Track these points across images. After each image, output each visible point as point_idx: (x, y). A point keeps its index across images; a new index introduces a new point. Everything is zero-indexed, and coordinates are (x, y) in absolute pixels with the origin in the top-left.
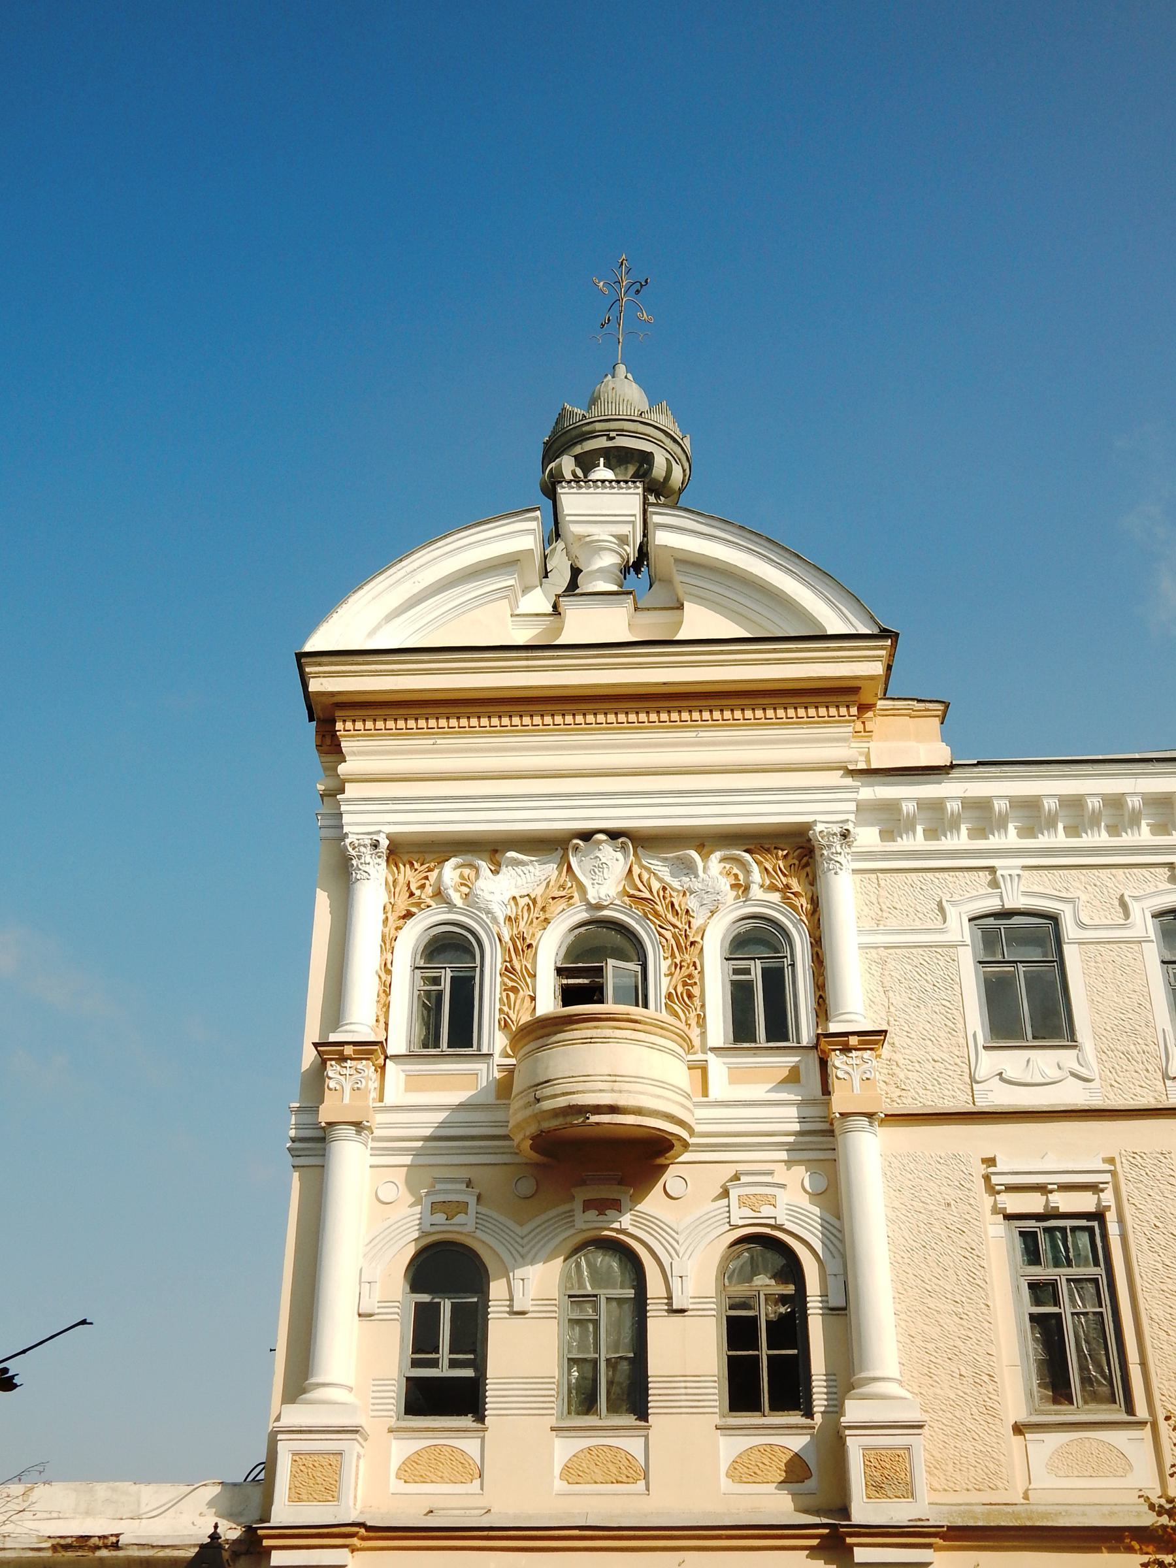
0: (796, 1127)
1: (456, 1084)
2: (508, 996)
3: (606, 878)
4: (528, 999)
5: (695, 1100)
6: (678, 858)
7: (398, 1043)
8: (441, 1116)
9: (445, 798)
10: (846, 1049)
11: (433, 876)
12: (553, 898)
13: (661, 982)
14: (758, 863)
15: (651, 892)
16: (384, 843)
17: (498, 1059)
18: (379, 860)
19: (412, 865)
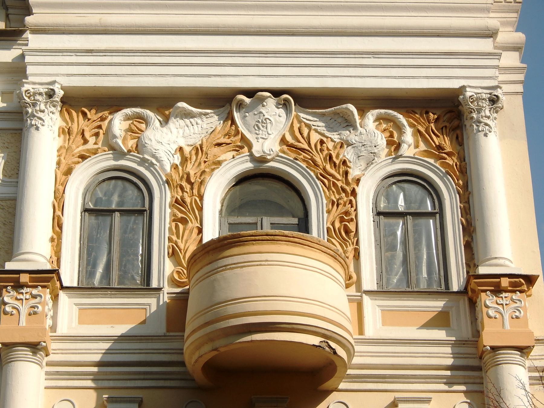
0: (450, 362)
1: (122, 317)
2: (177, 227)
3: (270, 133)
4: (196, 231)
5: (355, 337)
6: (335, 113)
7: (70, 275)
8: (107, 345)
9: (355, 53)
10: (497, 291)
11: (105, 124)
12: (219, 145)
13: (320, 217)
14: (411, 125)
15: (309, 144)
16: (60, 93)
17: (167, 289)
18: (53, 109)
19: (84, 114)
